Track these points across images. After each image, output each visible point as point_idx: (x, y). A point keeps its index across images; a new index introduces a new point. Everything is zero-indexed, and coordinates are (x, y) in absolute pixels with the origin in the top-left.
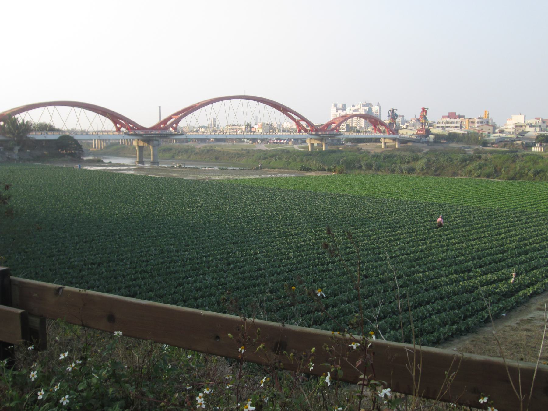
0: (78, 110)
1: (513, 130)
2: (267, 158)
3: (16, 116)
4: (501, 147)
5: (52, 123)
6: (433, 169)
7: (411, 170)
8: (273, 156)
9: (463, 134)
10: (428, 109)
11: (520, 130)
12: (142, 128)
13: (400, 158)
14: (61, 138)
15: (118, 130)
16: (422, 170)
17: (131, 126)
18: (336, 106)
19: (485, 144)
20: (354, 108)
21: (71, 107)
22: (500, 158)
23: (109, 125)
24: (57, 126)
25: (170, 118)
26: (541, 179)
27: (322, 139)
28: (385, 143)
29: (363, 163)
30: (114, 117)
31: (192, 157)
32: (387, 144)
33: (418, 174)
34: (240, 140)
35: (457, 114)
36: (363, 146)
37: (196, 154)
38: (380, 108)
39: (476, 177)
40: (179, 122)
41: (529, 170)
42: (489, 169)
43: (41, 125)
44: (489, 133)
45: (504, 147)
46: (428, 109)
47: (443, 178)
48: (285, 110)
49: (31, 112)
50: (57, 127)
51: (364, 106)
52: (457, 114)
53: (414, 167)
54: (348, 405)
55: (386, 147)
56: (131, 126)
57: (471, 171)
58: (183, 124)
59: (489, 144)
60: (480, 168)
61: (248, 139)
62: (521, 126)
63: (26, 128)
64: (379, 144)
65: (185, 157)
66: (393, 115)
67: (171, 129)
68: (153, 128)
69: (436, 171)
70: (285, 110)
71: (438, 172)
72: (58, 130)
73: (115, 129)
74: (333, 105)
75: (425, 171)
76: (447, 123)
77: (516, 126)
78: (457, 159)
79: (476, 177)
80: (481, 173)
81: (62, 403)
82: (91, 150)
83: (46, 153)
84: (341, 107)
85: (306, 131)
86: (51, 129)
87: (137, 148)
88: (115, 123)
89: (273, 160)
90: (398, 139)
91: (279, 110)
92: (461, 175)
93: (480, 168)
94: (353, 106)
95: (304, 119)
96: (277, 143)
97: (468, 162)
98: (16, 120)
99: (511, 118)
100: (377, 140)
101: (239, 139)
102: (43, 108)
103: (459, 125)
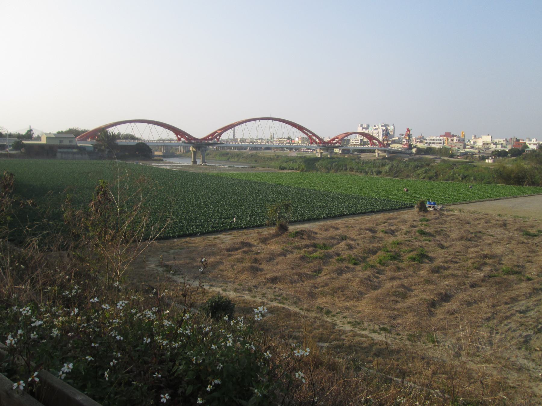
0: (151, 125)
1: (481, 147)
2: (288, 162)
3: (107, 130)
4: (464, 159)
5: (132, 134)
6: (394, 172)
7: (379, 173)
8: (291, 160)
9: (439, 148)
10: (411, 129)
11: (487, 146)
12: (195, 139)
13: (373, 164)
14: (138, 144)
15: (179, 139)
16: (386, 172)
17: (187, 137)
18: (361, 126)
19: (452, 156)
20: (375, 128)
21: (146, 124)
22: (442, 165)
23: (172, 136)
24: (137, 136)
25: (216, 132)
26: (467, 181)
27: (328, 149)
28: (379, 154)
29: (348, 167)
30: (177, 131)
31: (240, 160)
32: (380, 154)
33: (384, 175)
34: (282, 149)
35: (451, 134)
36: (363, 155)
37: (244, 158)
38: (394, 128)
39: (422, 179)
40: (221, 135)
41: (459, 175)
42: (432, 173)
43: (127, 135)
44: (459, 148)
45: (466, 159)
46: (411, 129)
47: (435, 183)
48: (301, 128)
49: (118, 126)
50: (137, 136)
51: (382, 126)
52: (451, 134)
53: (381, 171)
54: (395, 379)
55: (379, 156)
56: (187, 137)
57: (419, 174)
58: (225, 136)
59: (455, 156)
60: (426, 172)
61: (287, 148)
62: (487, 144)
63: (115, 137)
64: (374, 154)
65: (236, 160)
66: (387, 134)
67: (216, 139)
68: (205, 139)
69: (396, 173)
70: (301, 128)
71: (396, 175)
72: (137, 139)
73: (177, 138)
74: (360, 125)
75: (388, 174)
76: (433, 140)
77: (483, 144)
78: (411, 166)
79: (422, 179)
80: (425, 176)
81: (116, 331)
82: (177, 153)
83: (127, 154)
84: (365, 126)
85: (316, 143)
86: (133, 138)
87: (192, 152)
88: (177, 135)
89: (292, 163)
90: (388, 151)
91: (296, 128)
92: (412, 177)
93: (426, 172)
94: (375, 126)
95: (314, 135)
96: (308, 152)
97: (418, 168)
98: (107, 132)
99: (481, 138)
100: (373, 151)
101: (282, 148)
102: (128, 124)
103: (442, 142)
